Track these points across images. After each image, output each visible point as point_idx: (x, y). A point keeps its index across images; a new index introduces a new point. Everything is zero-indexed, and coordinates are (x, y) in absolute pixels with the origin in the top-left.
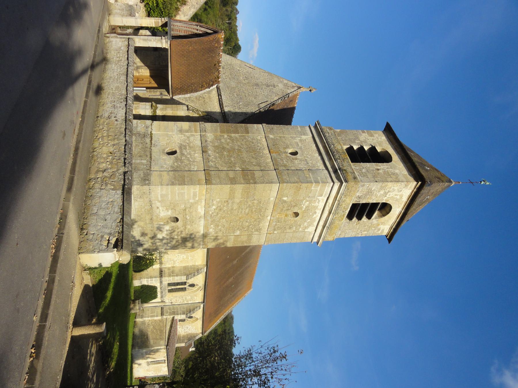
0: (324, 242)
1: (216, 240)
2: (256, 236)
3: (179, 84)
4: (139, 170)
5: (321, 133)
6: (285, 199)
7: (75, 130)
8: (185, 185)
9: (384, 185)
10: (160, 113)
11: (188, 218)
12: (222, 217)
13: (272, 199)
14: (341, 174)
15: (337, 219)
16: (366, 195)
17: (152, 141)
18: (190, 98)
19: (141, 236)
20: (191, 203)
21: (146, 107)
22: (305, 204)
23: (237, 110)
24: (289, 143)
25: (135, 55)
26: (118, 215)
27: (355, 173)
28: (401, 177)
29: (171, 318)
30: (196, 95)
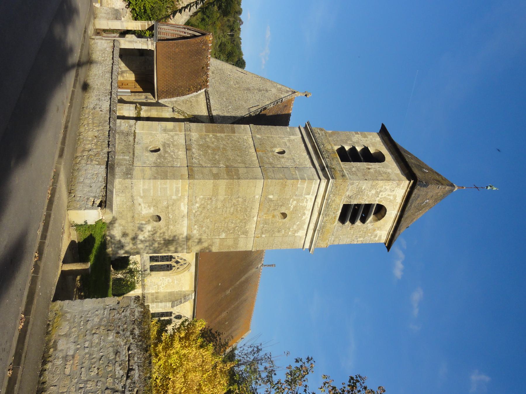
0: (315, 249)
1: (200, 244)
2: (242, 240)
3: (165, 87)
4: (121, 165)
5: (311, 133)
6: (271, 197)
7: (65, 111)
8: (167, 179)
9: (374, 183)
10: (144, 114)
11: (171, 217)
13: (257, 197)
14: (329, 171)
15: (328, 222)
16: (357, 195)
17: (135, 140)
18: (176, 101)
19: (122, 237)
20: (174, 199)
21: (130, 108)
23: (226, 114)
24: (276, 142)
25: (120, 59)
26: (101, 184)
27: (343, 171)
28: (393, 176)
30: (183, 98)
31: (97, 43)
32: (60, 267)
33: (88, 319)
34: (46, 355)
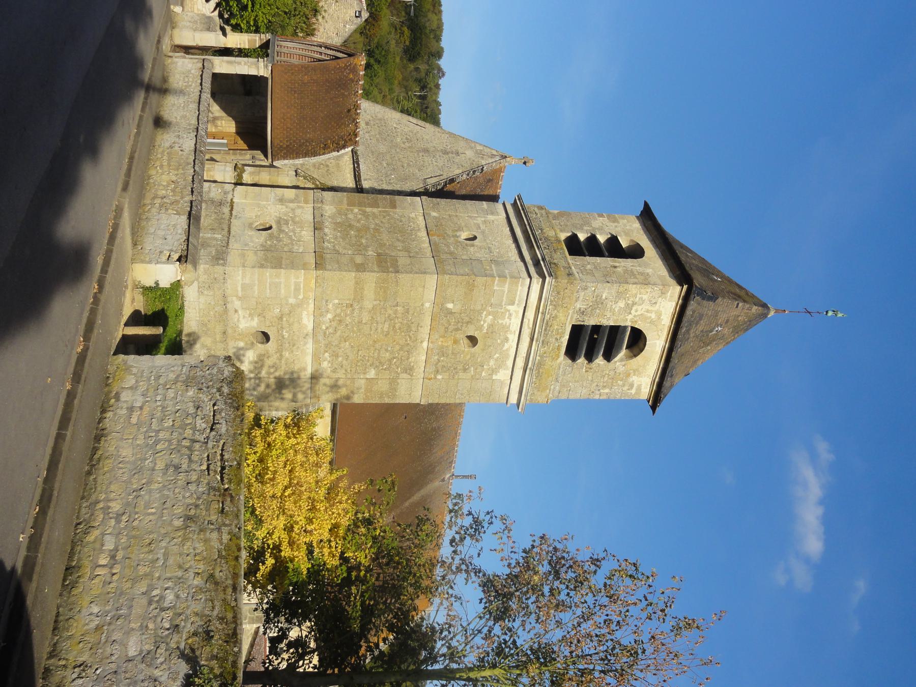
5: (522, 212)
6: (450, 306)
8: (281, 268)
9: (621, 289)
11: (286, 335)
12: (343, 337)
13: (427, 305)
14: (545, 266)
20: (291, 304)
22: (487, 320)
24: (463, 224)
25: (211, 100)
28: (653, 279)
29: (254, 629)
31: (177, 62)
32: (121, 329)
33: (161, 374)
34: (105, 405)
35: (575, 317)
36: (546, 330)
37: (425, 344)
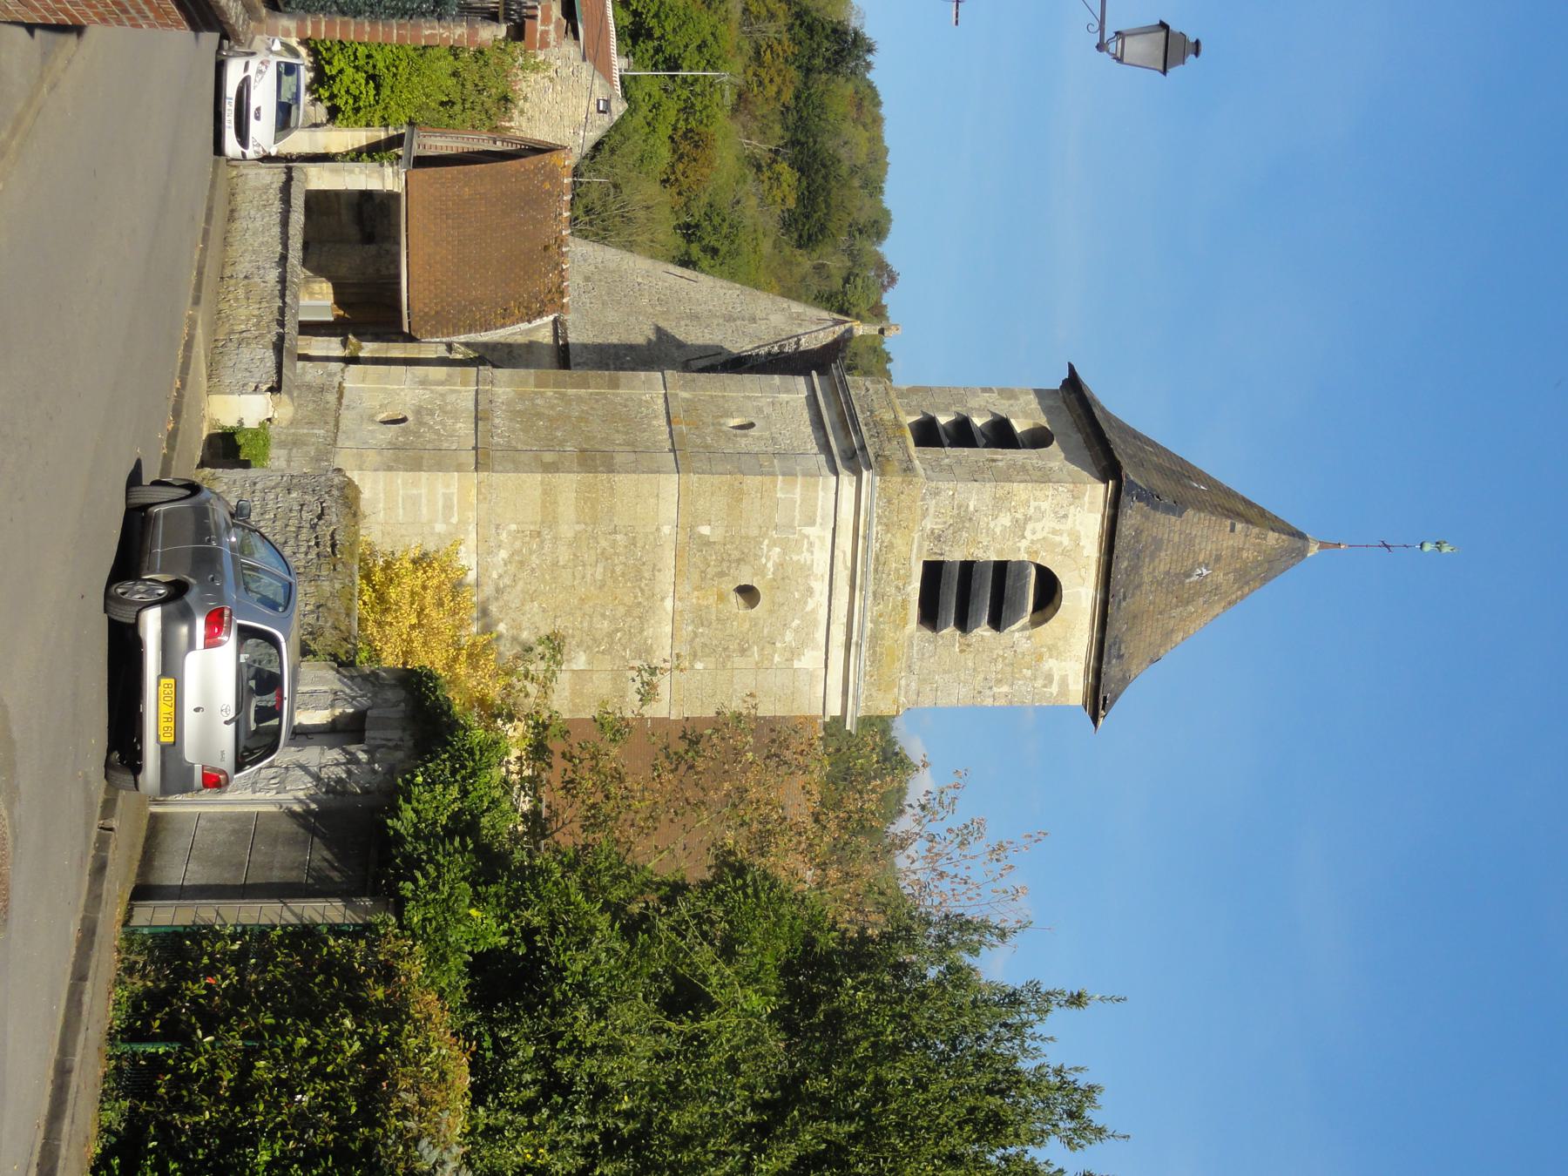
6: (705, 530)
9: (1000, 493)
13: (666, 529)
15: (886, 620)
31: (247, 175)
35: (926, 548)
36: (876, 570)
37: (668, 603)
